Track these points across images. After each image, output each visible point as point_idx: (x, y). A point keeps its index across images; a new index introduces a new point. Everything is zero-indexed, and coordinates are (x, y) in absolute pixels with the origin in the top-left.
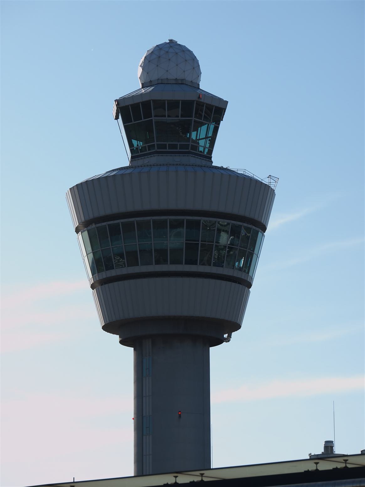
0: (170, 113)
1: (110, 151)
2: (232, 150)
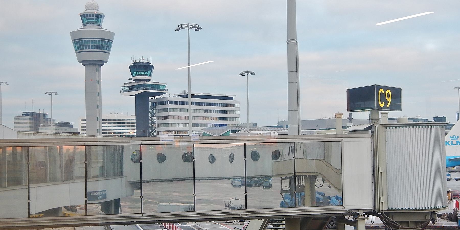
0: (92, 18)
1: (78, 25)
2: (106, 25)
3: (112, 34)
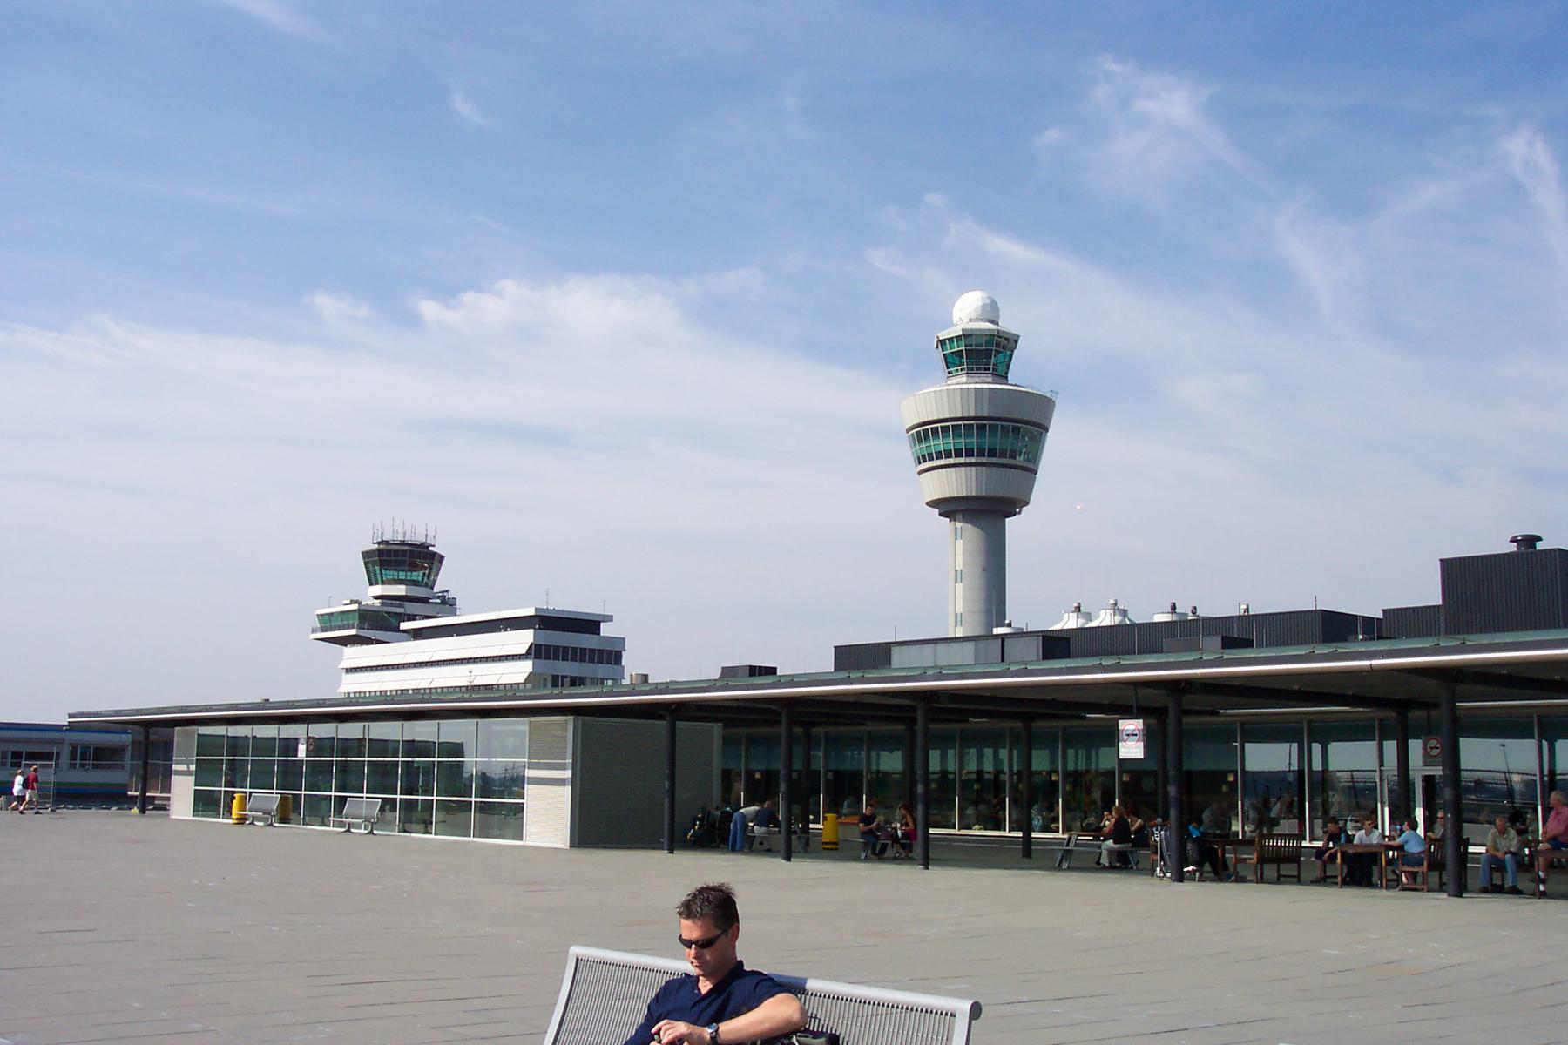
2: (1024, 374)
3: (1045, 405)
